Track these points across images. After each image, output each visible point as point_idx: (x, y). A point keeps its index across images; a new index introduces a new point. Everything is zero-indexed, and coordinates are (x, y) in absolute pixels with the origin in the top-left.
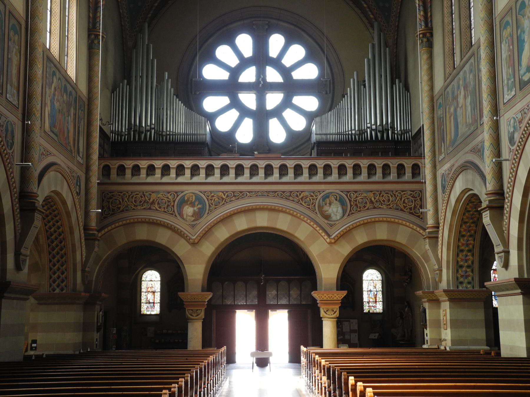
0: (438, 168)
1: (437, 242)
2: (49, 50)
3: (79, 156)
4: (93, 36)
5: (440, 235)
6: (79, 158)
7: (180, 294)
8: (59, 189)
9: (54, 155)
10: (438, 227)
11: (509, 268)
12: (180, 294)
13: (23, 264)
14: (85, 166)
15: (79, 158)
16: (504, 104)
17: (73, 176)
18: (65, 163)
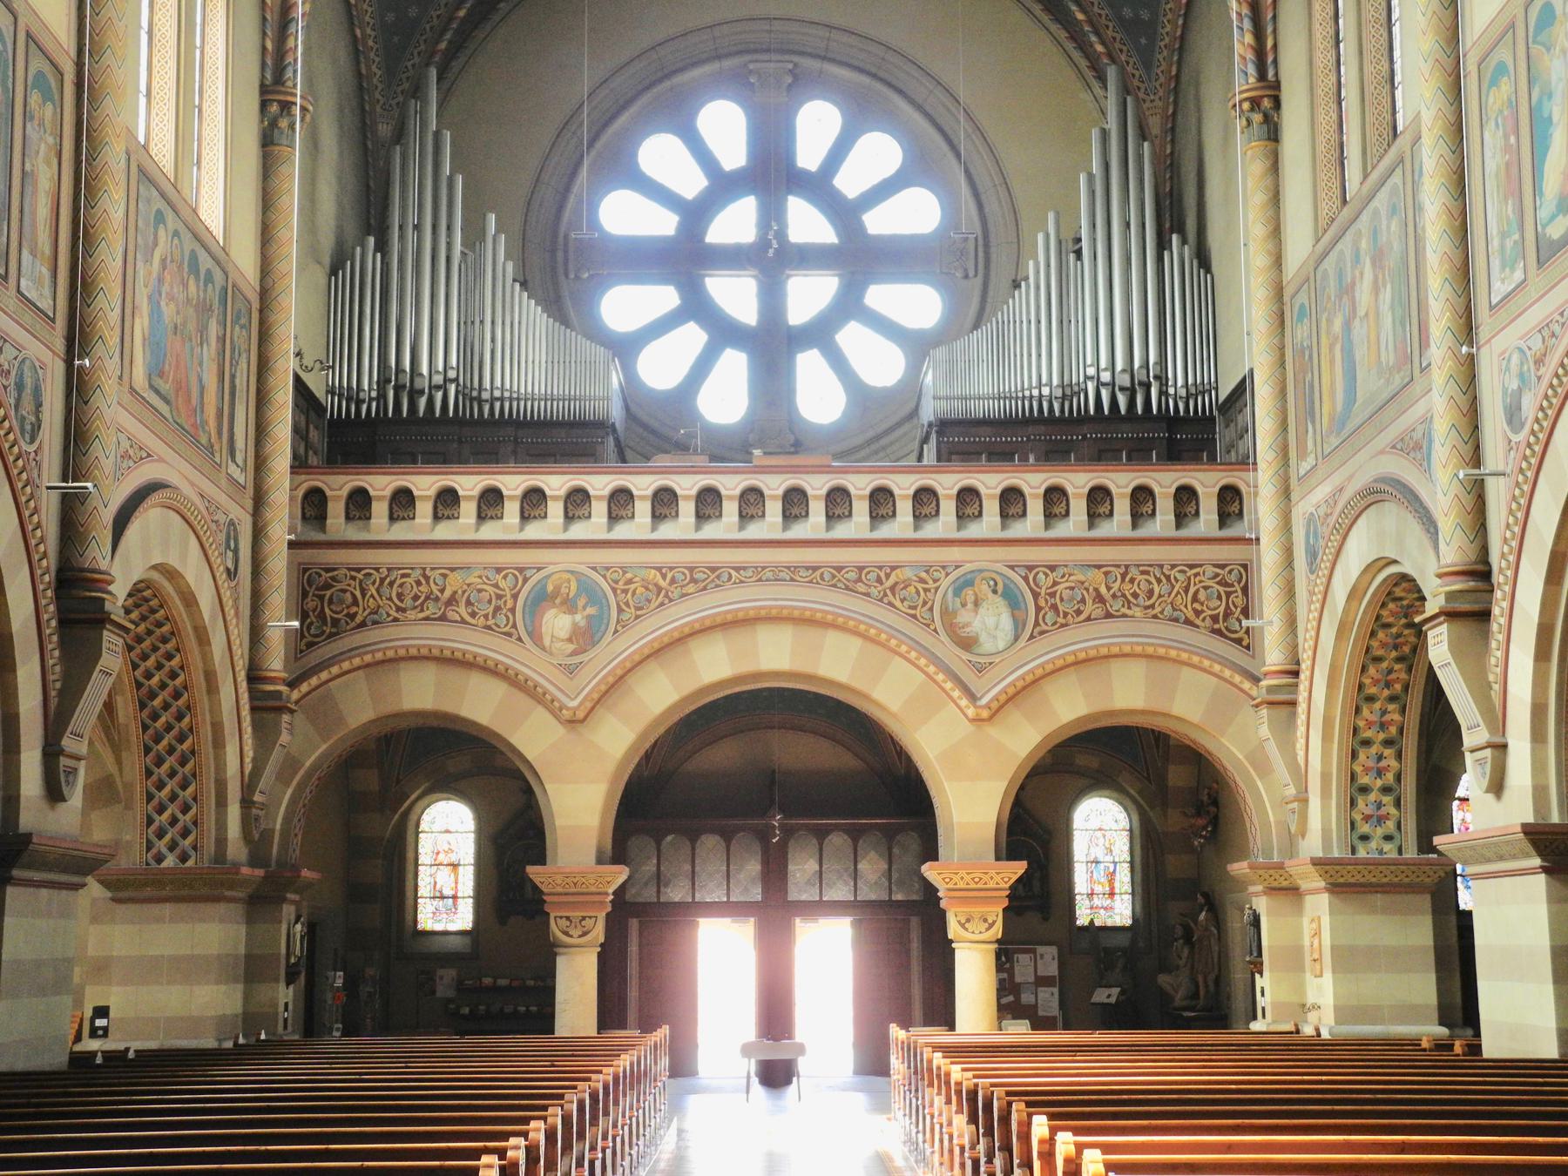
0: (1294, 496)
1: (1294, 715)
2: (145, 147)
3: (234, 460)
4: (274, 108)
5: (1302, 697)
6: (233, 469)
7: (532, 870)
8: (174, 561)
9: (161, 460)
10: (1296, 674)
11: (1507, 794)
12: (532, 870)
13: (67, 782)
14: (250, 491)
15: (233, 469)
16: (1491, 308)
17: (216, 522)
18: (192, 484)
